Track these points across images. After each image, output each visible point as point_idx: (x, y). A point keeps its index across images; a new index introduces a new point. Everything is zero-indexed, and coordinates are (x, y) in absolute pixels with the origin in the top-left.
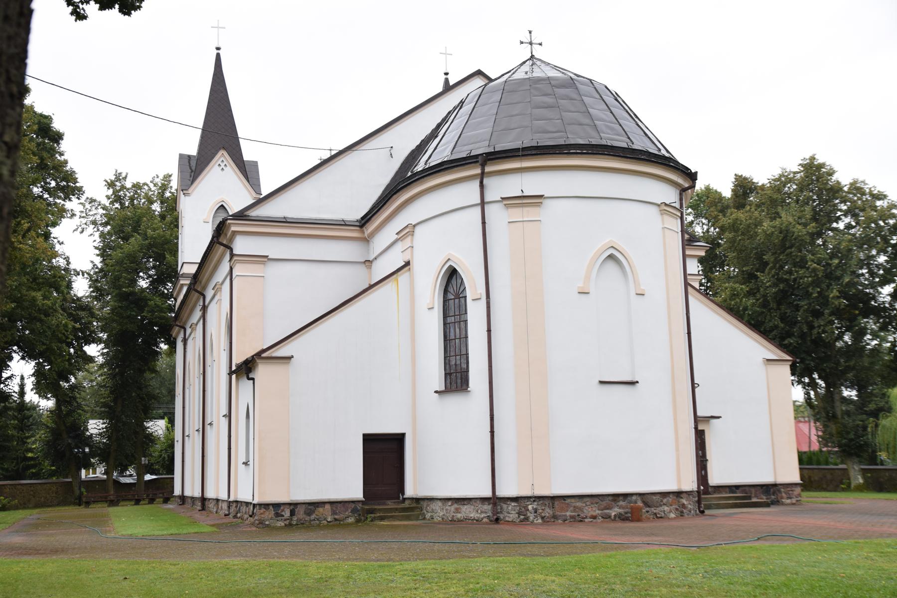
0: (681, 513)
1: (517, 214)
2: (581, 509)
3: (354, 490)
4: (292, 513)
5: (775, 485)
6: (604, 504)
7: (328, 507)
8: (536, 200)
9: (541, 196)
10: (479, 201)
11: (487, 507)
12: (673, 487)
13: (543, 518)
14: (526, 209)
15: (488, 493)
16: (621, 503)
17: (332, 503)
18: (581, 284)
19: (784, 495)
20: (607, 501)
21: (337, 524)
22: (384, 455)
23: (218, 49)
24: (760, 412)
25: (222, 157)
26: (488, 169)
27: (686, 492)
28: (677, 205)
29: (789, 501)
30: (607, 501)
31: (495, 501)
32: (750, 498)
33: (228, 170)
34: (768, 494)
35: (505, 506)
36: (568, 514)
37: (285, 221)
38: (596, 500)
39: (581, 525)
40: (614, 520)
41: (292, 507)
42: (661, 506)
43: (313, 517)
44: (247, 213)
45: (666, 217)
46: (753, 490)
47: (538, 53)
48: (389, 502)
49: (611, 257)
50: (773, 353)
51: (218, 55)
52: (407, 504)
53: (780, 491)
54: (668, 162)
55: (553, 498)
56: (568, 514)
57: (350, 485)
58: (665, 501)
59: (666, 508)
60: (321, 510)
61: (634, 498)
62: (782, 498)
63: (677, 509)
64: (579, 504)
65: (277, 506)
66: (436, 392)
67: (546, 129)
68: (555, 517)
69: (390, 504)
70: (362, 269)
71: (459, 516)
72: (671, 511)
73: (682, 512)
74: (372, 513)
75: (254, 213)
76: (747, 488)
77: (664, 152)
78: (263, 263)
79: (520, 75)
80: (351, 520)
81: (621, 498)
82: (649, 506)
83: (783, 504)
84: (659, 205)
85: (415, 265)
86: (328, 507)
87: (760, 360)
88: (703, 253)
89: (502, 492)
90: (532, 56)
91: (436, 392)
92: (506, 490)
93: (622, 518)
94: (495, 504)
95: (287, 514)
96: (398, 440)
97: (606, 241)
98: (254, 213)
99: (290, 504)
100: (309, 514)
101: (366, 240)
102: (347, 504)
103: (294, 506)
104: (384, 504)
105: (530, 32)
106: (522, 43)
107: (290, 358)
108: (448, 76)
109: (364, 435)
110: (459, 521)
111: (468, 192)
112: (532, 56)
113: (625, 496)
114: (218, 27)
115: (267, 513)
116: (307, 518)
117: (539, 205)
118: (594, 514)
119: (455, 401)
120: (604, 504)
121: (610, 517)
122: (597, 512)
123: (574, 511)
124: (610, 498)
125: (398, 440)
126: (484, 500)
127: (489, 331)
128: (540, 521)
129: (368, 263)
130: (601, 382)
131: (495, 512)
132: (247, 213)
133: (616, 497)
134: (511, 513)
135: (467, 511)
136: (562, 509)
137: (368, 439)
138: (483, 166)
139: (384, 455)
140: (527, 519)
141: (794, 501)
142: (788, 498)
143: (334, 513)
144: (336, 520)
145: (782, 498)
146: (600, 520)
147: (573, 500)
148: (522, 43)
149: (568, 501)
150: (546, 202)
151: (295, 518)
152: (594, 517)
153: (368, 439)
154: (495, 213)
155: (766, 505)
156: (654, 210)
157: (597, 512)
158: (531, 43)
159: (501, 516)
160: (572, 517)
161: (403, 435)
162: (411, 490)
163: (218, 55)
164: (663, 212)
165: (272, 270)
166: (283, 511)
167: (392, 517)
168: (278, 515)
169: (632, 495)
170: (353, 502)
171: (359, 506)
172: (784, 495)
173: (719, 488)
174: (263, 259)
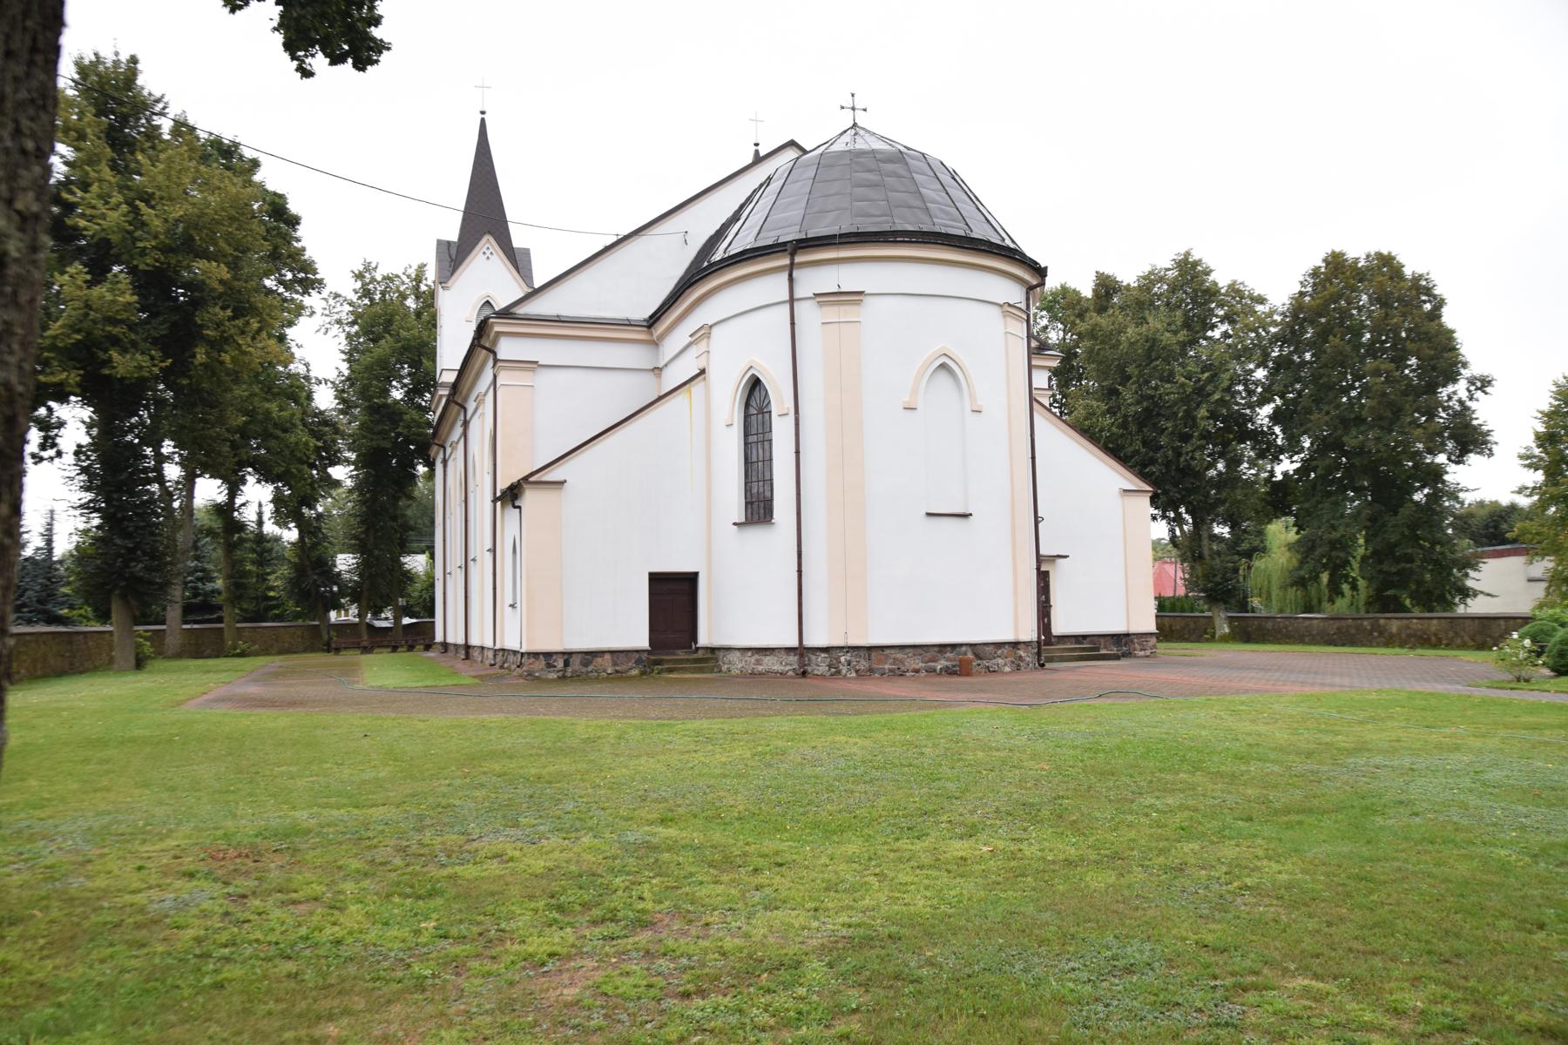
1: (832, 313)
2: (902, 662)
4: (567, 664)
5: (1128, 635)
7: (607, 656)
9: (861, 293)
10: (787, 297)
11: (793, 659)
12: (1010, 637)
15: (794, 643)
20: (932, 653)
21: (619, 677)
22: (674, 596)
24: (1113, 546)
25: (488, 244)
26: (798, 259)
28: (1023, 306)
31: (802, 651)
32: (1098, 649)
33: (495, 258)
34: (1120, 645)
37: (558, 320)
45: (826, 309)
49: (943, 366)
51: (483, 121)
52: (700, 654)
54: (1013, 255)
55: (870, 649)
57: (637, 636)
59: (1000, 661)
64: (900, 656)
65: (548, 655)
68: (871, 670)
70: (651, 377)
71: (760, 668)
75: (522, 310)
77: (1008, 242)
78: (533, 370)
79: (839, 147)
80: (635, 672)
85: (712, 374)
86: (607, 656)
89: (810, 641)
90: (855, 125)
92: (814, 639)
93: (949, 672)
94: (802, 655)
95: (560, 664)
96: (691, 579)
98: (522, 310)
99: (564, 653)
100: (586, 665)
101: (655, 344)
103: (568, 656)
107: (562, 483)
109: (651, 574)
110: (760, 674)
111: (776, 287)
112: (855, 125)
113: (954, 646)
119: (757, 534)
124: (738, 654)
125: (691, 579)
126: (789, 650)
127: (797, 452)
129: (657, 370)
130: (929, 514)
131: (802, 665)
133: (942, 647)
134: (820, 665)
135: (770, 663)
136: (880, 662)
137: (656, 579)
138: (792, 255)
139: (674, 596)
140: (839, 672)
143: (615, 664)
146: (923, 673)
149: (887, 652)
150: (868, 301)
151: (569, 670)
152: (917, 671)
153: (656, 579)
154: (805, 311)
155: (1117, 657)
156: (996, 311)
158: (853, 109)
161: (696, 574)
162: (704, 638)
163: (483, 121)
164: (1006, 314)
165: (544, 377)
168: (549, 666)
169: (962, 645)
173: (1063, 638)
174: (532, 366)
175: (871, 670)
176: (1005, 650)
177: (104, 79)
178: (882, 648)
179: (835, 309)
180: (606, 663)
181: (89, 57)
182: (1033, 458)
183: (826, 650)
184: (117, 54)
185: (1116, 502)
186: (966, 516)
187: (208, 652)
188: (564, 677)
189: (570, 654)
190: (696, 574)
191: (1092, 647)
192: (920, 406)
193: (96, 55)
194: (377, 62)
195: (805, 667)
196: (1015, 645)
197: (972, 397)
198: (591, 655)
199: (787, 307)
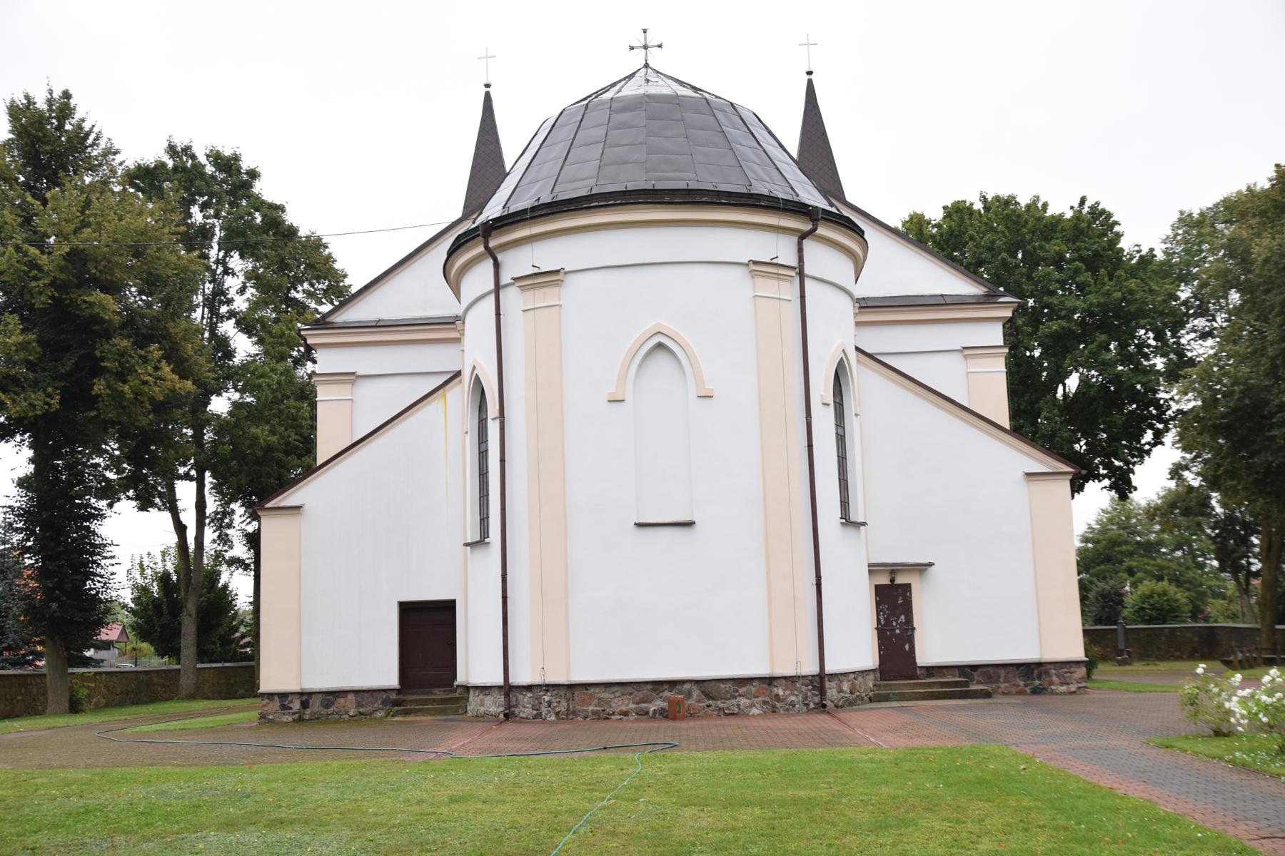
0: (772, 708)
2: (608, 703)
3: (390, 678)
4: (305, 705)
5: (1039, 664)
6: (640, 695)
7: (351, 697)
8: (547, 278)
9: (557, 272)
10: (492, 286)
12: (763, 671)
13: (557, 714)
14: (537, 291)
15: (500, 681)
16: (667, 694)
17: (356, 692)
18: (611, 389)
19: (1055, 679)
20: (646, 690)
21: (362, 717)
22: (427, 630)
23: (487, 86)
24: (1006, 552)
27: (785, 678)
29: (1064, 688)
30: (646, 690)
31: (508, 689)
32: (966, 684)
34: (1031, 677)
35: (520, 697)
36: (591, 708)
37: (378, 326)
38: (629, 689)
39: (603, 724)
40: (654, 717)
41: (305, 698)
42: (735, 697)
43: (330, 710)
44: (330, 319)
45: (760, 281)
46: (1002, 672)
47: (658, 60)
48: (436, 691)
49: (660, 346)
50: (1038, 462)
53: (1047, 673)
55: (571, 687)
56: (591, 708)
58: (742, 690)
60: (342, 701)
61: (687, 686)
62: (1052, 683)
63: (765, 703)
64: (605, 695)
65: (283, 695)
66: (466, 545)
67: (664, 165)
69: (439, 694)
72: (752, 706)
73: (774, 706)
74: (400, 705)
76: (991, 670)
78: (353, 383)
79: (630, 90)
81: (666, 687)
82: (713, 699)
83: (1053, 693)
84: (747, 265)
86: (351, 697)
87: (1021, 475)
88: (1009, 314)
89: (516, 679)
90: (646, 66)
91: (466, 545)
92: (521, 676)
93: (665, 715)
94: (507, 695)
95: (296, 705)
96: (448, 608)
97: (648, 326)
99: (301, 694)
100: (327, 707)
102: (376, 694)
103: (306, 697)
104: (431, 694)
105: (645, 31)
106: (632, 48)
107: (299, 508)
108: (812, 77)
112: (646, 66)
113: (673, 684)
114: (487, 57)
115: (271, 705)
116: (324, 711)
117: (558, 283)
118: (624, 708)
120: (640, 695)
121: (647, 713)
122: (632, 706)
123: (598, 704)
124: (649, 687)
125: (448, 608)
126: (500, 687)
128: (553, 718)
130: (639, 525)
131: (509, 706)
132: (330, 319)
133: (658, 685)
134: (525, 706)
136: (584, 702)
137: (407, 609)
139: (427, 630)
140: (539, 715)
141: (1073, 688)
142: (1062, 684)
143: (359, 705)
144: (361, 714)
145: (1052, 683)
146: (633, 717)
147: (597, 690)
148: (632, 48)
149: (592, 690)
151: (308, 711)
152: (626, 714)
153: (407, 609)
154: (512, 298)
155: (987, 695)
156: (740, 273)
157: (632, 706)
158: (646, 47)
159: (516, 711)
160: (594, 713)
161: (454, 601)
162: (461, 679)
164: (754, 274)
166: (291, 702)
167: (420, 710)
168: (284, 707)
169: (683, 682)
170: (385, 691)
171: (394, 696)
172: (1055, 679)
173: (931, 670)
174: (351, 378)
175: (575, 713)
176: (753, 688)
177: (39, 120)
178: (586, 686)
179: (773, 283)
180: (350, 704)
181: (20, 100)
182: (810, 446)
183: (529, 688)
184: (51, 92)
185: (1021, 492)
186: (689, 524)
187: (241, 691)
188: (301, 719)
189: (310, 694)
190: (454, 601)
191: (968, 682)
192: (629, 397)
193: (27, 97)
194: (1164, 242)
195: (578, 706)
196: (770, 681)
197: (699, 380)
198: (332, 696)
199: (492, 298)
